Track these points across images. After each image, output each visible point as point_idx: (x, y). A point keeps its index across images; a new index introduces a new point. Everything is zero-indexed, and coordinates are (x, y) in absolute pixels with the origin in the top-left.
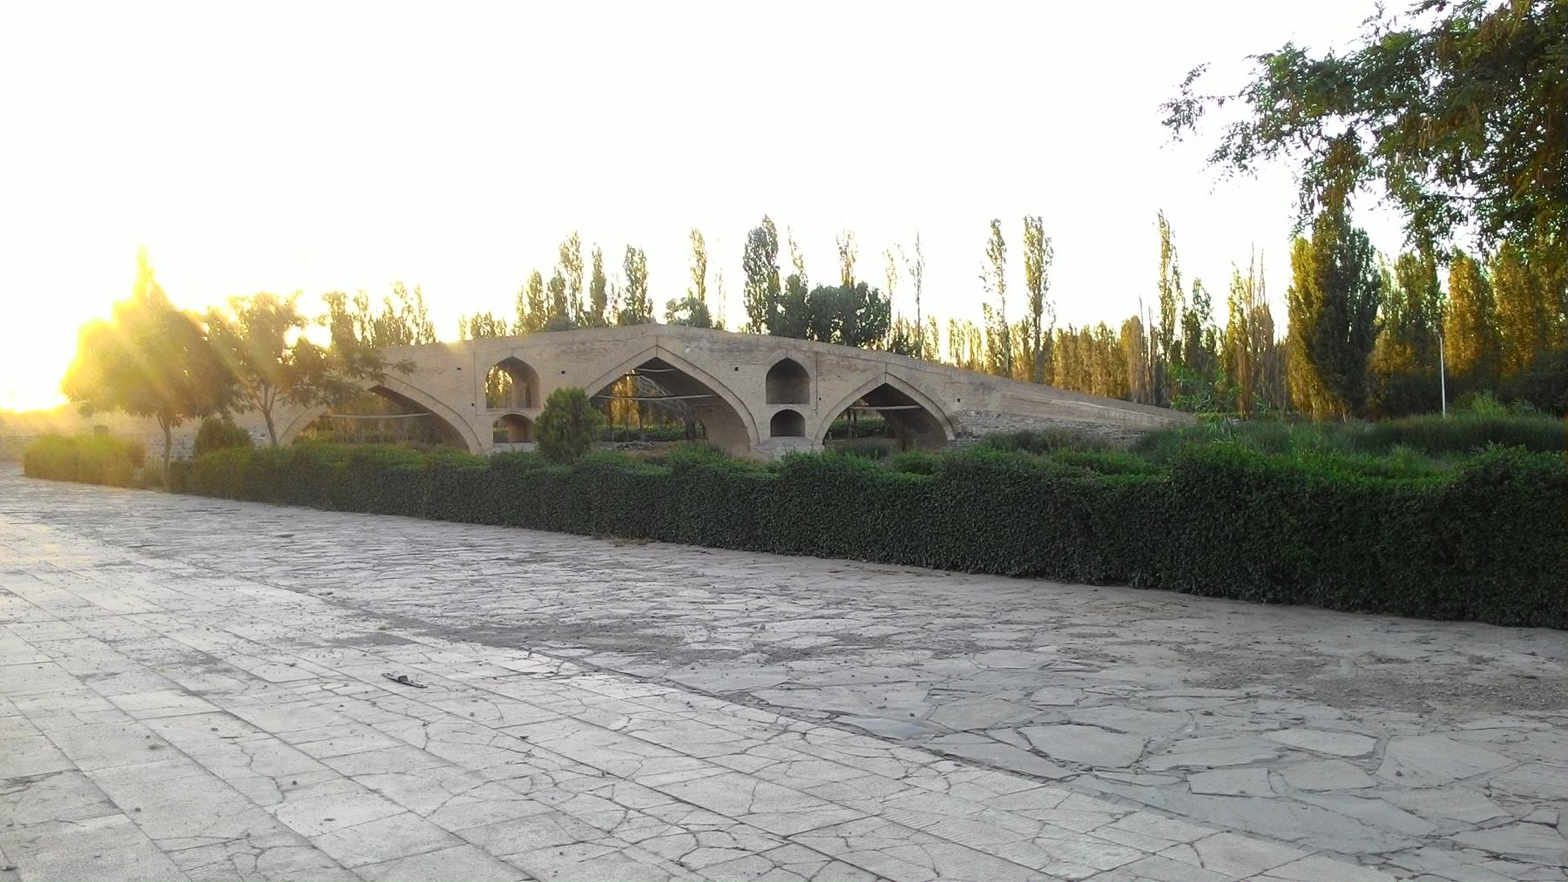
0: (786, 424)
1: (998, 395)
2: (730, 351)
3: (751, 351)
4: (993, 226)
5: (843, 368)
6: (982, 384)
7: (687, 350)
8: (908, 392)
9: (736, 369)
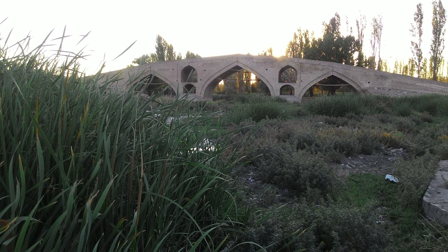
0: (189, 88)
1: (390, 81)
2: (265, 63)
3: (273, 63)
4: (418, 7)
5: (312, 69)
6: (382, 76)
7: (248, 63)
8: (343, 79)
9: (267, 69)
